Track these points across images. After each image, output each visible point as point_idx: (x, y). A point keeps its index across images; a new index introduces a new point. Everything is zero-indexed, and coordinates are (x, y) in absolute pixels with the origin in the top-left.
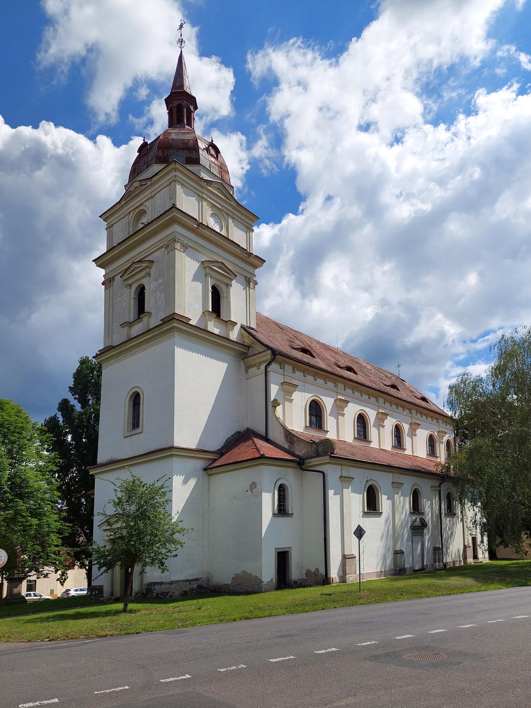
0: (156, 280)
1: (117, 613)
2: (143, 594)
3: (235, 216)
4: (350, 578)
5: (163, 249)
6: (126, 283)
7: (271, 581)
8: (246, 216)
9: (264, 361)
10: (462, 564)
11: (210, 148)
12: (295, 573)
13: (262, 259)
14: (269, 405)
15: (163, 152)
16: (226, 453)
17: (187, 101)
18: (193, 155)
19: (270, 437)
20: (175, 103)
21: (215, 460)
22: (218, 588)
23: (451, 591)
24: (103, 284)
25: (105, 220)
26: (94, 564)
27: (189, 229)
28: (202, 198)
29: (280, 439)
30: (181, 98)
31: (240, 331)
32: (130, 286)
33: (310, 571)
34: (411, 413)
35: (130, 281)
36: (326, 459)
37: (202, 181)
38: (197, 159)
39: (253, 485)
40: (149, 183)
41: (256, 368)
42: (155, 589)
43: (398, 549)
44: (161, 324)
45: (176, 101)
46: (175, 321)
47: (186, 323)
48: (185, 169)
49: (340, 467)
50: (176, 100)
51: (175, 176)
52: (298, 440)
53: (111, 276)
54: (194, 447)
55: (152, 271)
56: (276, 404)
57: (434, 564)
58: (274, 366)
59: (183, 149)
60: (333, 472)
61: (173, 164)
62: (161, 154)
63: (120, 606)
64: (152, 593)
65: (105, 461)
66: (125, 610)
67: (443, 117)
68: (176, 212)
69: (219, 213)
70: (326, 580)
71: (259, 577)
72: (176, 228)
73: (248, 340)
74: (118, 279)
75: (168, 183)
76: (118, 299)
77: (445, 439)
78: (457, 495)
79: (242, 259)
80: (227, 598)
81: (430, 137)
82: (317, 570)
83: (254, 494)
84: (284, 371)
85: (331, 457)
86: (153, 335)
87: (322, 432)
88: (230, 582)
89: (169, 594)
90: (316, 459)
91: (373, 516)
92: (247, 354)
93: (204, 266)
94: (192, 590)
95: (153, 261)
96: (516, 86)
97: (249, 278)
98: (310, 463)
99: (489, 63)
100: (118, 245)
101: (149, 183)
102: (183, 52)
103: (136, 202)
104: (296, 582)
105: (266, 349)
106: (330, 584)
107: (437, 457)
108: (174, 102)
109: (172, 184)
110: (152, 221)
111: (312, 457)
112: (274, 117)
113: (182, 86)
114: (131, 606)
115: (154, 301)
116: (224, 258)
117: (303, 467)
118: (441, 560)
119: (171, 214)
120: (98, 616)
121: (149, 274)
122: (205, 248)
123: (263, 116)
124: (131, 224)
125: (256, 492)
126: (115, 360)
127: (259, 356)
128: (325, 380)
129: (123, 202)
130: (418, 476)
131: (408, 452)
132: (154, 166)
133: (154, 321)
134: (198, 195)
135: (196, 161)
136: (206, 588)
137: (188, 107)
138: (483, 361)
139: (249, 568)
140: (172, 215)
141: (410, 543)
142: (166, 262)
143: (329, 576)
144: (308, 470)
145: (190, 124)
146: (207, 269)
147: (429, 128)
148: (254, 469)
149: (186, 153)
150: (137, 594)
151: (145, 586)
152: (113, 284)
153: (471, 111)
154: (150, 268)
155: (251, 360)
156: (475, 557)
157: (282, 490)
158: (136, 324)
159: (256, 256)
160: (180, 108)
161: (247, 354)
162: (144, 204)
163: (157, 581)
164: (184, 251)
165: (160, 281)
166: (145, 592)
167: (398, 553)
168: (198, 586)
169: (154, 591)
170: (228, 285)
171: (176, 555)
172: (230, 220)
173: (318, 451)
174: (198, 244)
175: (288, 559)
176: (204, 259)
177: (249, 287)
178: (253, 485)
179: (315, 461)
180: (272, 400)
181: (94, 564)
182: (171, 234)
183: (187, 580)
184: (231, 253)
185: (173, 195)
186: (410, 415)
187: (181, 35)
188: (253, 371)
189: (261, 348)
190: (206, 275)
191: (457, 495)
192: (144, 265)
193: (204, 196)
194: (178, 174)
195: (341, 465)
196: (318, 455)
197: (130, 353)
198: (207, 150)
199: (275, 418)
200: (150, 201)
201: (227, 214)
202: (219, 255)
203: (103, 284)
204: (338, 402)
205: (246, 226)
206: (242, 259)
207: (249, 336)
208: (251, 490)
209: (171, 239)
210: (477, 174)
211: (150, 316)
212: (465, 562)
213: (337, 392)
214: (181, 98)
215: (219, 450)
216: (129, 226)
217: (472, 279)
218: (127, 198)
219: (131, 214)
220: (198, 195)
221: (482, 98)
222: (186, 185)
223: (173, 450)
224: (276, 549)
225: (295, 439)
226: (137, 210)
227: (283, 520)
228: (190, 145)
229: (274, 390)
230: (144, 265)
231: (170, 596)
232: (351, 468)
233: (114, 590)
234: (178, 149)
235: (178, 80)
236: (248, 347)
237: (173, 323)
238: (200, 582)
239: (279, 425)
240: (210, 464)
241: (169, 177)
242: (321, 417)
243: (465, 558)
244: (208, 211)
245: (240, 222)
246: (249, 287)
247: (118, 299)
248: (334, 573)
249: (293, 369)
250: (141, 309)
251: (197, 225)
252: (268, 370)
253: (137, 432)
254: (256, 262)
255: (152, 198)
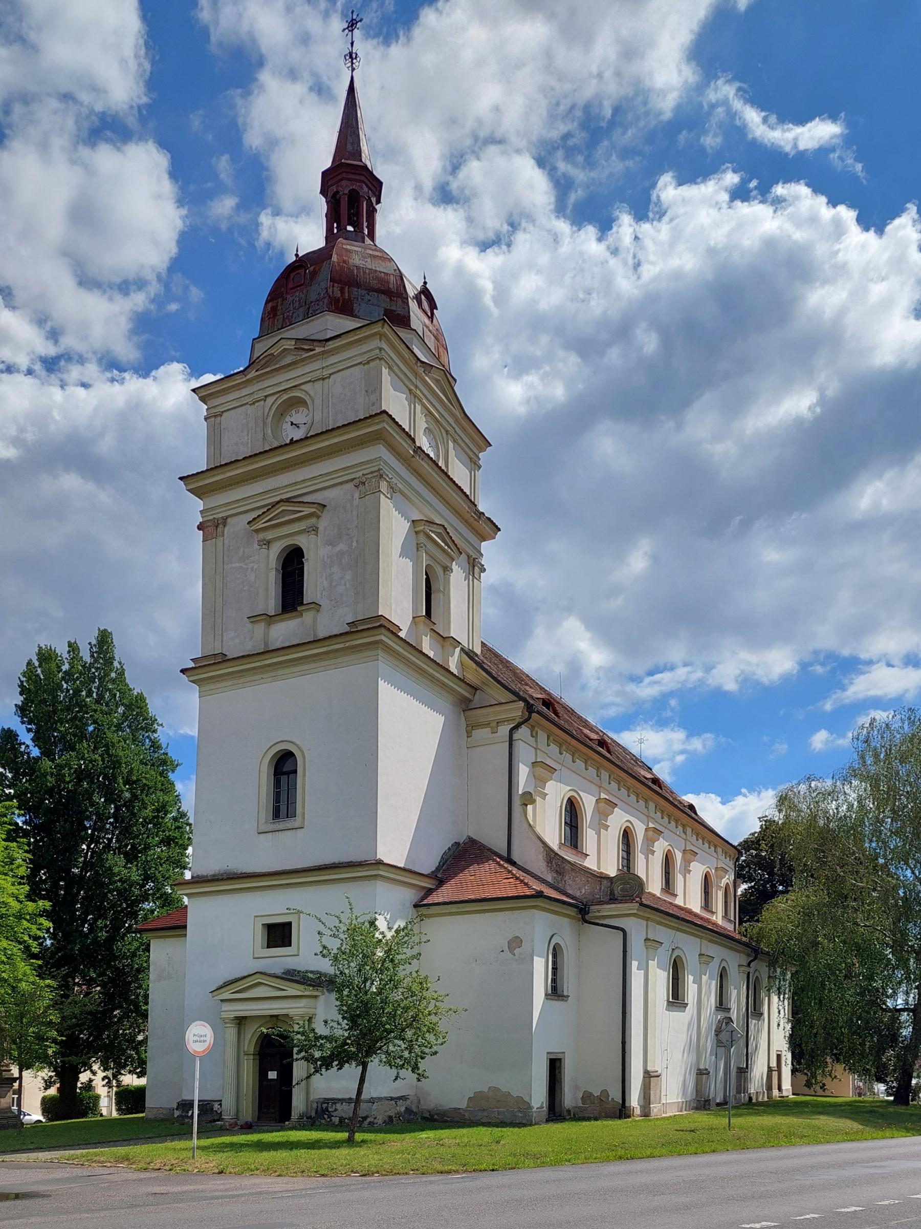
0: (331, 543)
1: (336, 1145)
2: (309, 1118)
3: (458, 438)
4: (655, 1110)
5: (350, 486)
6: (261, 536)
7: (542, 1107)
8: (472, 440)
9: (508, 720)
10: (766, 1099)
11: (423, 297)
12: (570, 1098)
13: (496, 527)
14: (515, 803)
15: (342, 291)
16: (449, 879)
17: (367, 186)
18: (398, 308)
19: (515, 857)
20: (345, 188)
21: (429, 892)
22: (438, 1114)
23: (830, 1136)
24: (199, 528)
25: (203, 399)
26: (297, 1060)
27: (399, 455)
28: (415, 396)
29: (538, 865)
30: (358, 177)
31: (460, 655)
32: (268, 543)
33: (591, 1094)
34: (685, 833)
35: (269, 535)
36: (633, 907)
37: (419, 364)
38: (404, 317)
39: (515, 943)
40: (318, 350)
41: (489, 729)
42: (336, 1110)
43: (702, 1067)
44: (346, 633)
45: (349, 183)
46: (383, 630)
47: (392, 632)
48: (393, 334)
49: (645, 922)
50: (349, 179)
51: (381, 349)
52: (572, 870)
53: (220, 515)
54: (402, 865)
55: (323, 524)
56: (528, 798)
57: (738, 1096)
58: (524, 731)
59: (380, 291)
60: (637, 929)
61: (380, 324)
62: (338, 294)
63: (345, 1135)
64: (330, 1116)
65: (211, 873)
66: (350, 1142)
67: (593, 212)
68: (388, 424)
69: (436, 427)
70: (623, 1111)
71: (526, 1099)
72: (380, 451)
73: (474, 675)
74: (238, 524)
75: (364, 358)
76: (237, 565)
77: (723, 884)
78: (765, 981)
79: (466, 521)
80: (483, 1130)
81: (565, 248)
82: (605, 1092)
83: (517, 957)
84: (536, 741)
85: (641, 904)
86: (329, 648)
87: (580, 855)
88: (463, 1105)
89: (369, 1120)
90: (608, 906)
91: (677, 1009)
92: (470, 701)
93: (417, 529)
94: (399, 1115)
95: (325, 506)
96: (731, 178)
97: (474, 559)
98: (599, 911)
99: (691, 117)
100: (244, 459)
101: (318, 350)
102: (355, 79)
103: (284, 379)
104: (569, 1111)
105: (515, 698)
106: (629, 1117)
107: (713, 913)
108: (344, 183)
109: (372, 364)
110: (333, 429)
111: (601, 903)
112: (253, 140)
113: (358, 154)
114: (359, 1136)
115: (326, 583)
116: (446, 520)
117: (587, 917)
118: (745, 1090)
119: (377, 423)
120: (320, 1148)
121: (315, 530)
122: (420, 495)
123: (231, 137)
124: (270, 419)
125: (521, 954)
126: (230, 683)
127: (497, 708)
128: (586, 763)
129: (253, 374)
130: (726, 946)
131: (679, 901)
132: (328, 317)
133: (329, 622)
134: (410, 390)
135: (403, 321)
136: (415, 1114)
137: (369, 198)
138: (652, 726)
139: (508, 1084)
140: (375, 426)
141: (714, 1057)
142: (355, 513)
143: (627, 1104)
144: (598, 924)
145: (372, 235)
146: (421, 536)
147: (563, 226)
148: (517, 914)
149: (384, 299)
150: (301, 1117)
151: (315, 1105)
152: (223, 533)
153: (644, 208)
154: (318, 517)
155: (481, 715)
156: (780, 1089)
157: (556, 952)
158: (278, 621)
159: (489, 519)
160: (354, 199)
161: (470, 701)
162: (303, 387)
163: (340, 1097)
164: (391, 499)
165: (342, 546)
166: (313, 1114)
167: (701, 1073)
168: (406, 1108)
169: (334, 1114)
170: (447, 569)
171: (436, 1053)
172: (451, 444)
173: (612, 893)
174: (410, 485)
175: (560, 1072)
176: (417, 516)
177: (473, 576)
178: (515, 943)
179: (608, 909)
180: (520, 792)
181: (297, 1060)
182: (371, 461)
183: (392, 1099)
184: (457, 512)
185: (374, 388)
186: (684, 836)
187: (352, 44)
188: (481, 734)
189: (502, 695)
190: (418, 547)
191: (765, 981)
192: (307, 510)
193: (418, 392)
194: (384, 345)
195: (647, 919)
196: (613, 899)
197: (271, 674)
198: (417, 297)
199: (526, 825)
200: (318, 385)
201: (447, 432)
202: (440, 514)
203: (199, 528)
204: (603, 804)
205: (471, 459)
206: (466, 521)
207: (478, 669)
208: (511, 949)
209: (372, 472)
210: (648, 342)
211: (318, 611)
212: (770, 1096)
213: (600, 787)
214: (358, 177)
215: (432, 872)
216: (264, 423)
217: (638, 562)
218: (262, 368)
219: (270, 401)
220: (410, 390)
221: (668, 190)
222: (395, 368)
223: (381, 867)
224: (548, 1053)
225: (568, 867)
226: (285, 397)
227: (556, 1004)
228: (391, 286)
229: (523, 772)
230: (307, 510)
231: (370, 1123)
232: (658, 926)
233: (240, 1109)
234: (370, 289)
235: (350, 140)
236: (475, 689)
237: (368, 632)
238: (408, 1102)
239: (534, 839)
240: (423, 898)
241: (365, 348)
242: (577, 828)
243: (769, 1088)
244: (422, 423)
245: (463, 449)
246: (473, 576)
247: (237, 565)
248: (634, 1101)
249: (548, 739)
250: (292, 595)
251: (414, 451)
252: (515, 736)
253: (289, 825)
254: (488, 529)
255: (324, 379)
